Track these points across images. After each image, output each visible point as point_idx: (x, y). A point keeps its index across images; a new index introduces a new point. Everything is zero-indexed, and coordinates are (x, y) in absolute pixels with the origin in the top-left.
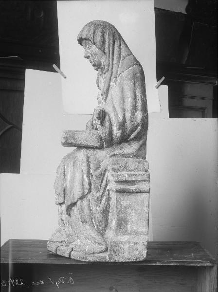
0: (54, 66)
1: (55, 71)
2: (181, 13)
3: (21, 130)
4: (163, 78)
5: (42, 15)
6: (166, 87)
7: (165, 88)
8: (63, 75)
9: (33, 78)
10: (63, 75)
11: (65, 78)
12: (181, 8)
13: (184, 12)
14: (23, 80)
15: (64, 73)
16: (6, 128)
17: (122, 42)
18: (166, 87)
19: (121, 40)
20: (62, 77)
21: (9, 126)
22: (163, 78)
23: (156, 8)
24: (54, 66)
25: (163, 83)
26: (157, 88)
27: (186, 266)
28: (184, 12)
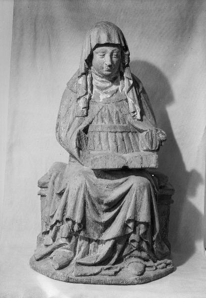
17: (87, 97)
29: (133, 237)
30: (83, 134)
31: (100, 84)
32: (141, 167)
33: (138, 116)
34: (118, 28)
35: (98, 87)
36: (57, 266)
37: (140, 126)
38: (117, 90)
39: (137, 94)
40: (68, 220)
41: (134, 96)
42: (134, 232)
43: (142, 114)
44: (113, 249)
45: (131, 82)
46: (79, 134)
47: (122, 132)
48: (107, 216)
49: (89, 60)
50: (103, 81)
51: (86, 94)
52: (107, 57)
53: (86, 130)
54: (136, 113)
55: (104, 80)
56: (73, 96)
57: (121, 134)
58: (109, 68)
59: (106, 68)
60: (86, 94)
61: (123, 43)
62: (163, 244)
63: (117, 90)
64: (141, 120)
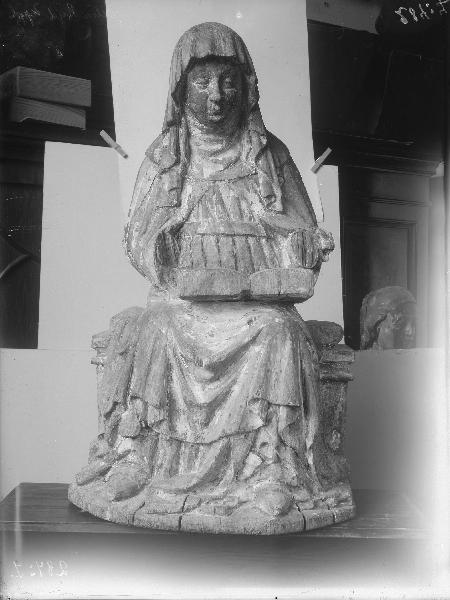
0: (103, 133)
1: (106, 144)
2: (365, 32)
3: (38, 260)
4: (329, 151)
5: (89, 35)
6: (335, 169)
7: (332, 171)
8: (121, 152)
9: (58, 157)
10: (121, 152)
11: (126, 157)
12: (364, 20)
13: (373, 30)
14: (40, 164)
15: (123, 149)
16: (17, 260)
17: (179, 169)
18: (335, 169)
19: (179, 169)
20: (120, 156)
21: (22, 257)
22: (329, 151)
23: (310, 22)
24: (103, 133)
25: (327, 162)
26: (316, 172)
27: (349, 538)
28: (373, 30)
29: (263, 437)
30: (169, 237)
31: (204, 147)
32: (277, 293)
33: (278, 206)
34: (235, 33)
35: (200, 152)
36: (112, 496)
37: (283, 223)
38: (238, 159)
39: (275, 164)
40: (134, 398)
41: (268, 164)
42: (311, 476)
43: (284, 201)
44: (225, 456)
45: (264, 141)
46: (162, 237)
47: (247, 236)
48: (215, 389)
49: (180, 93)
50: (211, 141)
51: (177, 162)
52: (213, 85)
53: (177, 231)
54: (273, 199)
55: (212, 137)
56: (153, 172)
57: (244, 239)
58: (217, 108)
59: (213, 107)
60: (177, 162)
61: (240, 53)
62: (264, 341)
63: (238, 159)
64: (284, 212)
